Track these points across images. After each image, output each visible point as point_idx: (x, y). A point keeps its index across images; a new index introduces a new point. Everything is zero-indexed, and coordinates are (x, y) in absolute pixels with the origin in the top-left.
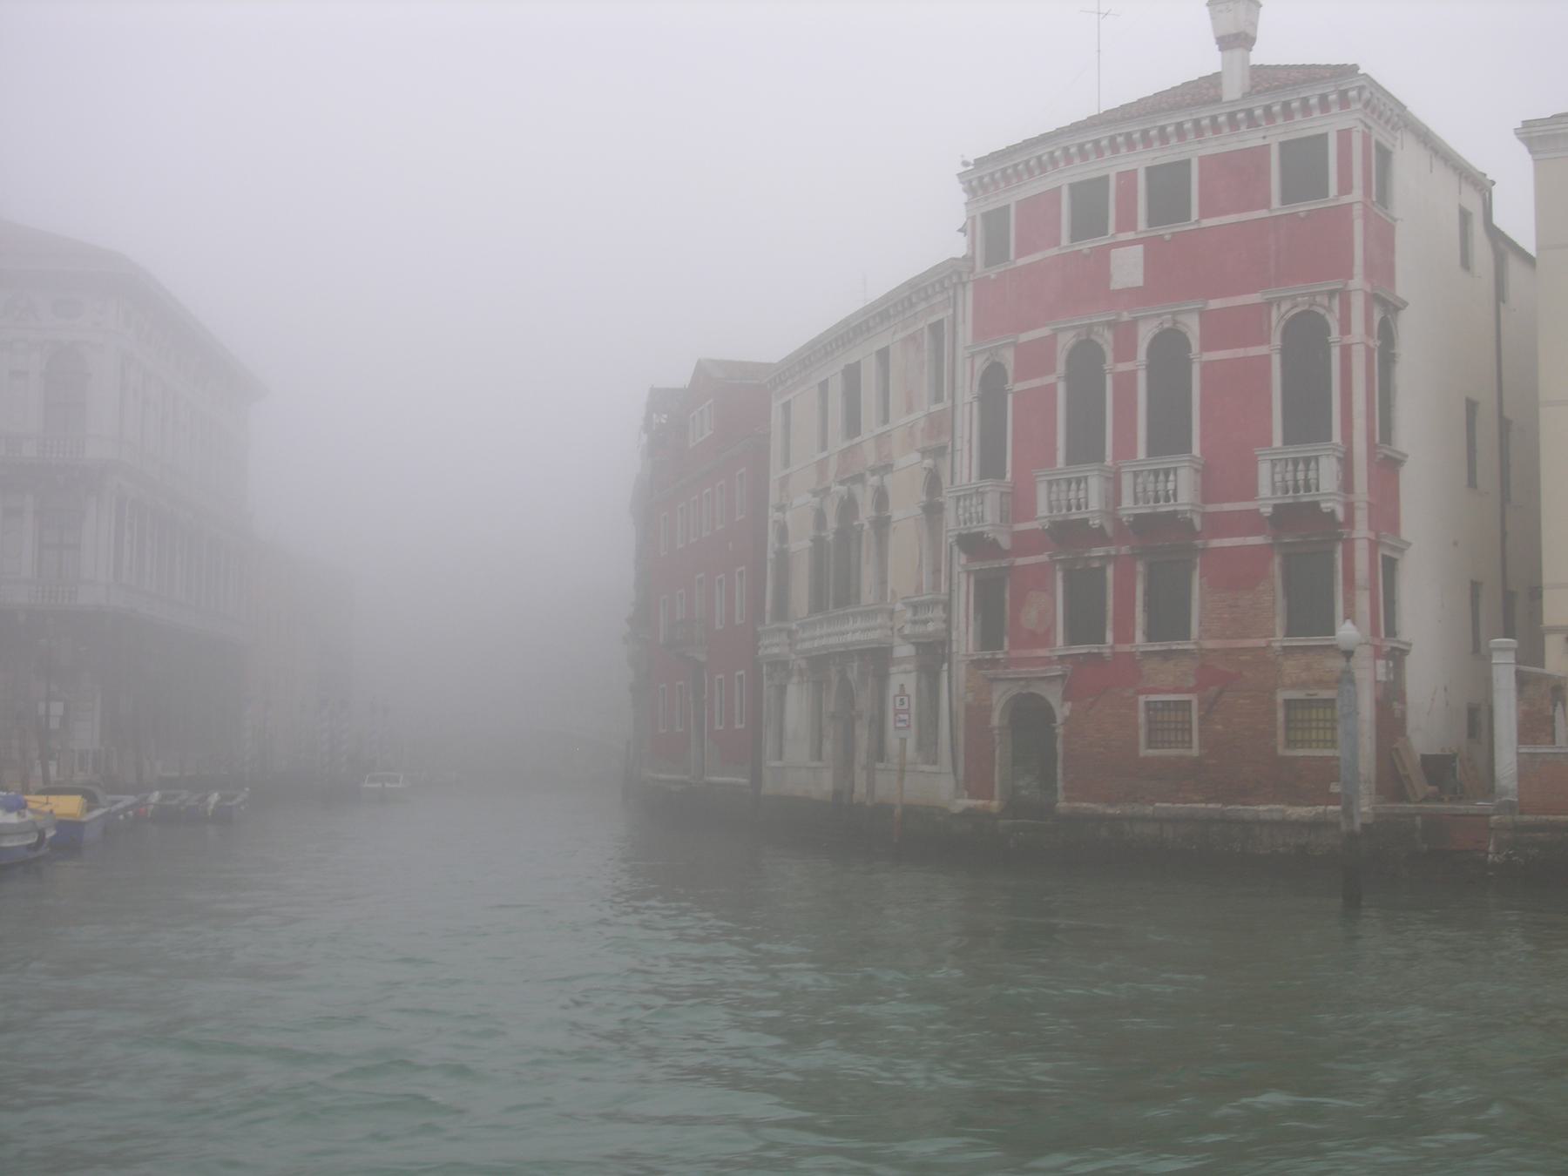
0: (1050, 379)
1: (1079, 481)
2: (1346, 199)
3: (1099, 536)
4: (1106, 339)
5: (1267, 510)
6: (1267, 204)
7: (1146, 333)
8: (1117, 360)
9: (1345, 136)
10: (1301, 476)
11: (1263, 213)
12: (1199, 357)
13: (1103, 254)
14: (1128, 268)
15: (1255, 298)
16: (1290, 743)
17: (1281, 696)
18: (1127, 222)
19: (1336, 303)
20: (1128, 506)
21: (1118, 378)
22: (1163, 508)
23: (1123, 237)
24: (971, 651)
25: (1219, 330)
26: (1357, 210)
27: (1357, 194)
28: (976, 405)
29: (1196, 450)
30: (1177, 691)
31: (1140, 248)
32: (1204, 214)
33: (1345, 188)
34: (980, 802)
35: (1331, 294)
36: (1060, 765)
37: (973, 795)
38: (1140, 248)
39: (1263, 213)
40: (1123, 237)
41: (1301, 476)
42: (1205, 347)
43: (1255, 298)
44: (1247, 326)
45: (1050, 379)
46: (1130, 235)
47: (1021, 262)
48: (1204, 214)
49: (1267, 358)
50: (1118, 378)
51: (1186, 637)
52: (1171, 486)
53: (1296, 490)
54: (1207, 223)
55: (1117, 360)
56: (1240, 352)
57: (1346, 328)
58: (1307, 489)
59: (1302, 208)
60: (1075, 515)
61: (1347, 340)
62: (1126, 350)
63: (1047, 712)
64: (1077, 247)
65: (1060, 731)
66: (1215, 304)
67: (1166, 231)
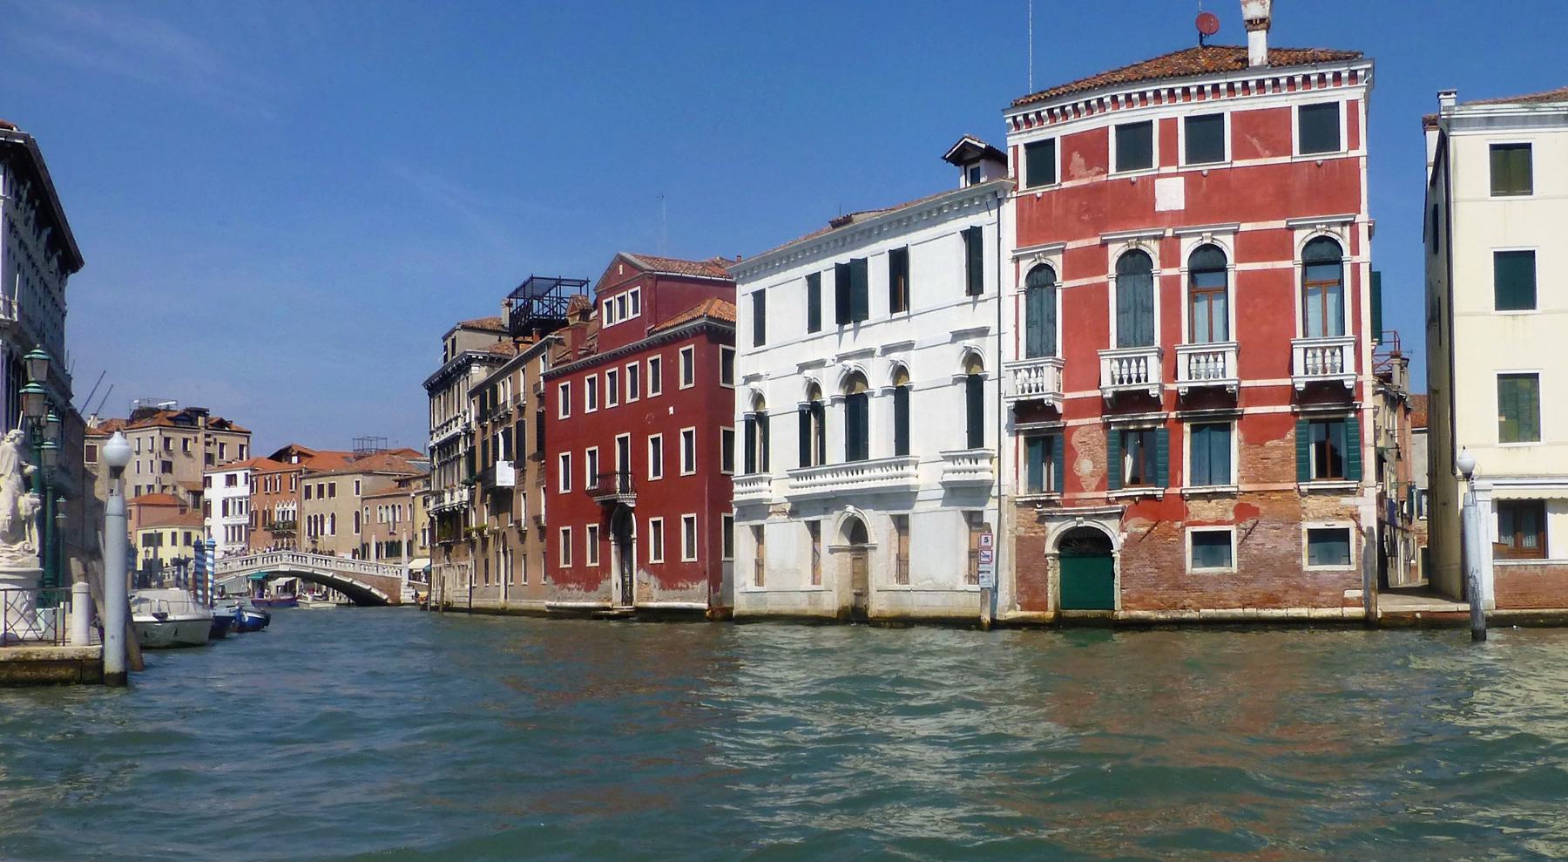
0: (1103, 279)
1: (1138, 361)
2: (1352, 153)
3: (1154, 404)
4: (1153, 249)
5: (1300, 386)
6: (1289, 152)
7: (1188, 246)
8: (1163, 266)
9: (1353, 105)
10: (1328, 360)
11: (1287, 159)
12: (1062, 283)
13: (1148, 184)
14: (1170, 194)
15: (1281, 224)
16: (1046, 609)
17: (1308, 525)
18: (1169, 157)
19: (1347, 229)
20: (1183, 384)
21: (1165, 281)
22: (1135, 387)
23: (1165, 170)
24: (1022, 492)
25: (1076, 263)
26: (1363, 162)
27: (1362, 151)
28: (1022, 298)
29: (1059, 355)
30: (1218, 523)
31: (1181, 179)
32: (1236, 156)
33: (1354, 144)
34: (1034, 614)
35: (1344, 224)
36: (1117, 581)
37: (1025, 607)
38: (1181, 179)
39: (1287, 159)
40: (1165, 170)
41: (1134, 370)
42: (1065, 278)
43: (1281, 224)
44: (1278, 245)
45: (1103, 279)
46: (1173, 169)
47: (1066, 185)
48: (1236, 156)
49: (1178, 277)
50: (1165, 281)
51: (1228, 480)
52: (1220, 365)
53: (1325, 371)
54: (1237, 164)
55: (1163, 266)
56: (1268, 265)
57: (1355, 250)
58: (1138, 380)
59: (1319, 157)
60: (1332, 377)
61: (1356, 259)
62: (1171, 258)
63: (1104, 542)
64: (1125, 175)
65: (1117, 556)
66: (1245, 227)
67: (1204, 168)
